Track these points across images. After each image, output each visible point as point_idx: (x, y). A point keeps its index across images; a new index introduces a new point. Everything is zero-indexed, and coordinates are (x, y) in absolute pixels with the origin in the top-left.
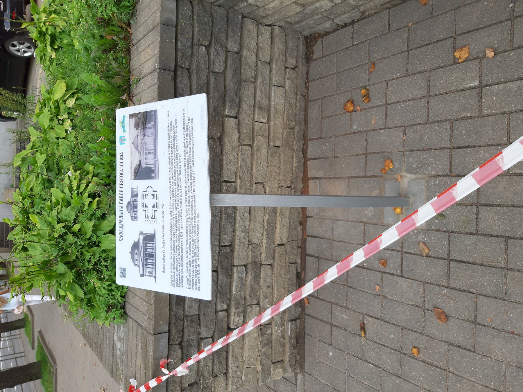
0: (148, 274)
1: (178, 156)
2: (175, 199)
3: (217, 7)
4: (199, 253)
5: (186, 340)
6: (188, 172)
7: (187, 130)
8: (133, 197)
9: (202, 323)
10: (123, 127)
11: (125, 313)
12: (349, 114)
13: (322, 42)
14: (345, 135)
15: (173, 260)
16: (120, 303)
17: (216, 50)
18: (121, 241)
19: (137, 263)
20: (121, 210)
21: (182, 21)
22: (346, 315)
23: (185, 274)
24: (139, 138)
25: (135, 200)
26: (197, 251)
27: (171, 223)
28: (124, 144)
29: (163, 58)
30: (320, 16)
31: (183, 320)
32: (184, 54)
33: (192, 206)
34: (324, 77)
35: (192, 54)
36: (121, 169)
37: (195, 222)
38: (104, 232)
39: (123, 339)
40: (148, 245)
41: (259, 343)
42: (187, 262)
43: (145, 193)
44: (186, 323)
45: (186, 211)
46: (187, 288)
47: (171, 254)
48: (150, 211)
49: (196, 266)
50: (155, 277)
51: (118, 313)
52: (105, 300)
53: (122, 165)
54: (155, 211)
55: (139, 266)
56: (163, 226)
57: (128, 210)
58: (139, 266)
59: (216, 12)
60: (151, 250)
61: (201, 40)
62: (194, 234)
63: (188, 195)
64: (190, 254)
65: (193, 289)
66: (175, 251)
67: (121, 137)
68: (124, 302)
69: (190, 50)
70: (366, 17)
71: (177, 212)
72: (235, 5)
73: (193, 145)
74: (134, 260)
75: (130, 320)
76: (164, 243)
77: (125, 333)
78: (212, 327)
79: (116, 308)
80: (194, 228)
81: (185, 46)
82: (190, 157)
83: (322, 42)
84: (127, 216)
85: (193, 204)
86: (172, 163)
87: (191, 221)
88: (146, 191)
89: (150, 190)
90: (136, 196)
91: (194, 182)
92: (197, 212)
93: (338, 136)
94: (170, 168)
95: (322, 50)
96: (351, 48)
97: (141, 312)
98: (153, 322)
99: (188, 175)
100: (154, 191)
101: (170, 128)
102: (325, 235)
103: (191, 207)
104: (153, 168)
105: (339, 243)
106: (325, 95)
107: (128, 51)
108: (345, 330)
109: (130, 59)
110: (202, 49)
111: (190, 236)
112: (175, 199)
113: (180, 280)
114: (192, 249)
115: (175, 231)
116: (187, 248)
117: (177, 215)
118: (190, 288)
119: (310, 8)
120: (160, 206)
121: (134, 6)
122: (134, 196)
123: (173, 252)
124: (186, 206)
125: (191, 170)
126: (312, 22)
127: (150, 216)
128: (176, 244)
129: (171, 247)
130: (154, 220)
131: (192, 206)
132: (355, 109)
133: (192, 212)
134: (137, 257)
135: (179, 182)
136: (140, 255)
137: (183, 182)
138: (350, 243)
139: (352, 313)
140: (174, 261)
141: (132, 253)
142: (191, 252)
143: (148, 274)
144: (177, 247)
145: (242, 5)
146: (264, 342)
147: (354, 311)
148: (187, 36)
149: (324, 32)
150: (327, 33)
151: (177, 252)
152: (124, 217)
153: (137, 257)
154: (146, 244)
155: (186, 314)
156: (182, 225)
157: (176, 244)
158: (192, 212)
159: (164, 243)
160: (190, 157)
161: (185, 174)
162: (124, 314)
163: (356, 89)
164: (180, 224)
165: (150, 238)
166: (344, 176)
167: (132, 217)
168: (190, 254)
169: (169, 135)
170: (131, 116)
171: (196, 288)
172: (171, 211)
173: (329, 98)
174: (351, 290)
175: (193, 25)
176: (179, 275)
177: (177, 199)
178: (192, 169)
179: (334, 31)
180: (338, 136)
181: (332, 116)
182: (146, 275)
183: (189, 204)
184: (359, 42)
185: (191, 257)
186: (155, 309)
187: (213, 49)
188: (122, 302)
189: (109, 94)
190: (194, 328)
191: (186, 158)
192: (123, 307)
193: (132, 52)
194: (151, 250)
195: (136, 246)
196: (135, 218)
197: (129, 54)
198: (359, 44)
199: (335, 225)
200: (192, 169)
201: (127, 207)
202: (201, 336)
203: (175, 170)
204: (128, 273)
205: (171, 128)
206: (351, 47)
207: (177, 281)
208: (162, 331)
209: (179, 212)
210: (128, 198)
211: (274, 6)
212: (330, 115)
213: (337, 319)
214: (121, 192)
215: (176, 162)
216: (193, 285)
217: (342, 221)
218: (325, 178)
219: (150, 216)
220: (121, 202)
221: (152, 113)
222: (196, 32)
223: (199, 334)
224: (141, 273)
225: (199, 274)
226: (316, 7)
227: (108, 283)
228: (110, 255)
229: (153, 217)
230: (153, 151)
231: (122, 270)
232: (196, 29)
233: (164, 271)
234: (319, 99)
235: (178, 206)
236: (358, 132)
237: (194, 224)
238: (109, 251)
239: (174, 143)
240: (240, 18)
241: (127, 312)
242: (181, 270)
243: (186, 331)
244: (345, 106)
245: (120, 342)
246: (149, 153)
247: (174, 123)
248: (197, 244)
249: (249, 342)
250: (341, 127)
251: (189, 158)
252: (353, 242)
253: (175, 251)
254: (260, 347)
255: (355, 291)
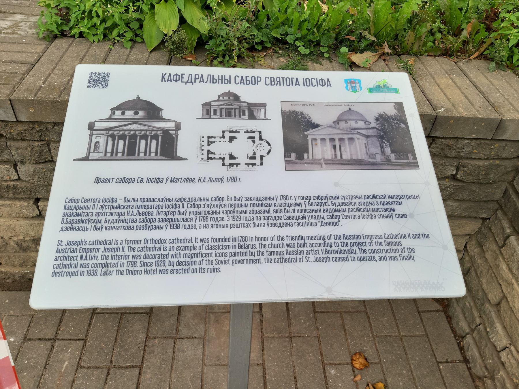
0: (94, 140)
1: (334, 219)
2: (249, 209)
3: (504, 189)
4: (134, 273)
5: (9, 143)
6: (304, 245)
7: (389, 244)
8: (249, 109)
9: (41, 166)
10: (377, 89)
11: (56, 37)
12: (349, 361)
13: (438, 311)
14: (322, 355)
15: (122, 203)
16: (71, 29)
17: (448, 187)
18: (163, 77)
19: (118, 113)
20: (223, 80)
21: (497, 145)
22: (67, 367)
23: (91, 235)
24: (361, 124)
25: (244, 114)
26: (138, 268)
27: (200, 199)
28: (347, 88)
29: (452, 121)
30: (478, 321)
31: (41, 140)
32: (449, 147)
33: (235, 254)
34: (394, 315)
35: (447, 157)
36: (301, 81)
37: (201, 263)
38: (182, 8)
39: (13, 33)
40: (154, 142)
41: (22, 238)
42: (116, 242)
43: (257, 135)
44: (37, 144)
45: (226, 240)
46: (60, 243)
47: (135, 200)
48: (222, 148)
49: (107, 265)
50: (86, 159)
51: (54, 27)
52: (76, 6)
53: (308, 83)
54: (223, 159)
55: (110, 119)
56: (192, 180)
57: (223, 95)
58: (110, 119)
59: (498, 188)
60: (142, 149)
61: (465, 169)
62: (175, 260)
63: (257, 244)
64: (133, 250)
65: (57, 259)
66: (141, 211)
67: (359, 82)
68: (73, 36)
69: (453, 154)
70: (474, 382)
71: (221, 215)
72: (505, 214)
73: (361, 259)
74: (124, 106)
75: (43, 47)
76: (158, 180)
77: (22, 37)
78: (36, 179)
79: (62, 24)
80: (187, 260)
81: (462, 148)
82: (336, 252)
83: (438, 311)
84: (212, 92)
85: (239, 258)
86: (319, 205)
87: (204, 251)
88: (261, 139)
89: (263, 149)
90: (252, 116)
91: (286, 261)
92: (222, 267)
93: (319, 341)
94: (309, 198)
95: (428, 311)
96: (434, 359)
97: (53, 70)
98: (30, 97)
99: (300, 246)
100: (262, 157)
101: (388, 200)
102: (183, 325)
103: (232, 251)
104: (305, 155)
105: (171, 351)
106: (371, 317)
107: (447, 53)
108: (46, 364)
109: (435, 56)
110: (452, 170)
111: (171, 249)
112: (249, 209)
113: (78, 222)
114: (143, 253)
115: (182, 210)
116: (146, 242)
117: (215, 216)
118: (58, 251)
119: (493, 314)
120: (234, 172)
121: (512, 67)
122: (252, 111)
123: (139, 203)
124: (234, 239)
125: (308, 253)
126: (467, 304)
127: (212, 148)
128: (155, 211)
129: (149, 200)
130: (205, 156)
131: (235, 254)
132: (357, 372)
133: (221, 255)
134: (129, 114)
135: (283, 221)
136: (134, 121)
137: (284, 232)
138: (172, 369)
139: (70, 379)
140: (119, 207)
141: (137, 104)
142: (136, 253)
143: (94, 140)
144: (149, 214)
145: (506, 224)
146: (23, 243)
147: (74, 381)
148: (475, 151)
149: (450, 314)
150: (449, 318)
151: (139, 214)
152: (209, 86)
153: (129, 114)
154: (156, 137)
155: (52, 144)
156: (194, 227)
157: (155, 211)
158: (221, 255)
159: (158, 180)
160: (336, 252)
161: (301, 237)
162: (52, 37)
163: (383, 370)
164: (198, 223)
165: (168, 147)
166: (266, 356)
167: (209, 104)
168: (133, 250)
169: (374, 197)
170: (399, 106)
171: (58, 266)
172: (222, 199)
173: (367, 325)
174: (103, 376)
175: (487, 159)
176: (89, 221)
177: (248, 215)
178: (312, 257)
179: (454, 331)
180: (319, 341)
181: (345, 330)
182: (91, 136)
183: (240, 247)
184: (443, 374)
185: (127, 253)
186: (54, 101)
187: (448, 184)
188: (73, 32)
189: (394, 26)
190: (30, 156)
191: (332, 241)
192: (63, 35)
193: (444, 59)
194: (142, 149)
195: (153, 111)
196: (208, 113)
197: (443, 55)
198: (441, 372)
199: (196, 341)
200: (312, 257)
201: (229, 94)
202: (19, 166)
203: (306, 211)
204: (96, 91)
205: (389, 203)
206: (436, 359)
207: (77, 215)
208: (17, 111)
209: (222, 219)
210: (248, 94)
211: (502, 269)
212: (346, 328)
213: (62, 350)
214: (256, 81)
215: (321, 214)
216: (66, 258)
217: (204, 355)
218: (262, 321)
219: (212, 148)
220: (238, 80)
221: (411, 159)
222: (477, 162)
223: (22, 163)
224: (97, 125)
225: (89, 273)
226: (494, 323)
227: (101, 13)
228: (147, 17)
229: (210, 156)
230: (339, 157)
231: (103, 77)
232: (481, 163)
233: (98, 181)
234: (365, 308)
235: (234, 219)
236: (326, 377)
237: (198, 260)
238: (153, 14)
239: (359, 210)
240: (484, 216)
241: (57, 41)
242: (99, 225)
243: (24, 144)
244: (360, 354)
245: (10, 27)
246: (334, 147)
247: (399, 210)
248: (154, 268)
249: (21, 225)
250: (332, 346)
251: (334, 248)
252: (173, 376)
253: (141, 211)
254: (15, 239)
255: (102, 382)
